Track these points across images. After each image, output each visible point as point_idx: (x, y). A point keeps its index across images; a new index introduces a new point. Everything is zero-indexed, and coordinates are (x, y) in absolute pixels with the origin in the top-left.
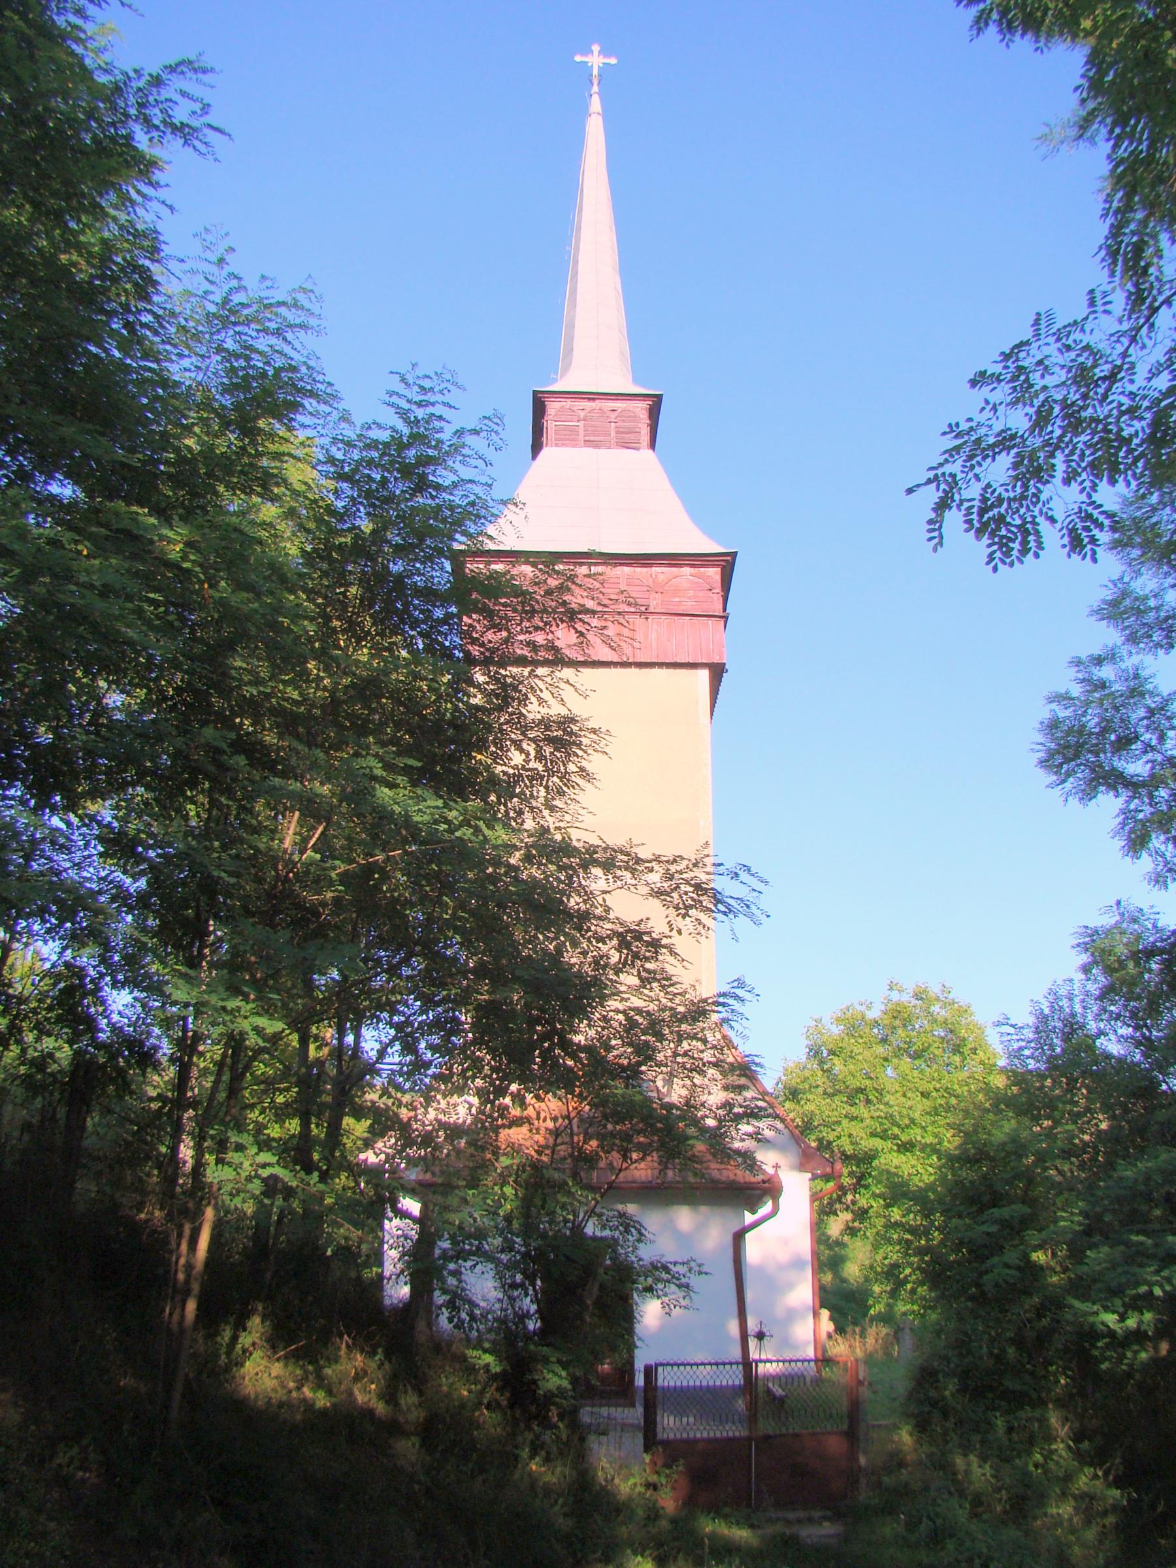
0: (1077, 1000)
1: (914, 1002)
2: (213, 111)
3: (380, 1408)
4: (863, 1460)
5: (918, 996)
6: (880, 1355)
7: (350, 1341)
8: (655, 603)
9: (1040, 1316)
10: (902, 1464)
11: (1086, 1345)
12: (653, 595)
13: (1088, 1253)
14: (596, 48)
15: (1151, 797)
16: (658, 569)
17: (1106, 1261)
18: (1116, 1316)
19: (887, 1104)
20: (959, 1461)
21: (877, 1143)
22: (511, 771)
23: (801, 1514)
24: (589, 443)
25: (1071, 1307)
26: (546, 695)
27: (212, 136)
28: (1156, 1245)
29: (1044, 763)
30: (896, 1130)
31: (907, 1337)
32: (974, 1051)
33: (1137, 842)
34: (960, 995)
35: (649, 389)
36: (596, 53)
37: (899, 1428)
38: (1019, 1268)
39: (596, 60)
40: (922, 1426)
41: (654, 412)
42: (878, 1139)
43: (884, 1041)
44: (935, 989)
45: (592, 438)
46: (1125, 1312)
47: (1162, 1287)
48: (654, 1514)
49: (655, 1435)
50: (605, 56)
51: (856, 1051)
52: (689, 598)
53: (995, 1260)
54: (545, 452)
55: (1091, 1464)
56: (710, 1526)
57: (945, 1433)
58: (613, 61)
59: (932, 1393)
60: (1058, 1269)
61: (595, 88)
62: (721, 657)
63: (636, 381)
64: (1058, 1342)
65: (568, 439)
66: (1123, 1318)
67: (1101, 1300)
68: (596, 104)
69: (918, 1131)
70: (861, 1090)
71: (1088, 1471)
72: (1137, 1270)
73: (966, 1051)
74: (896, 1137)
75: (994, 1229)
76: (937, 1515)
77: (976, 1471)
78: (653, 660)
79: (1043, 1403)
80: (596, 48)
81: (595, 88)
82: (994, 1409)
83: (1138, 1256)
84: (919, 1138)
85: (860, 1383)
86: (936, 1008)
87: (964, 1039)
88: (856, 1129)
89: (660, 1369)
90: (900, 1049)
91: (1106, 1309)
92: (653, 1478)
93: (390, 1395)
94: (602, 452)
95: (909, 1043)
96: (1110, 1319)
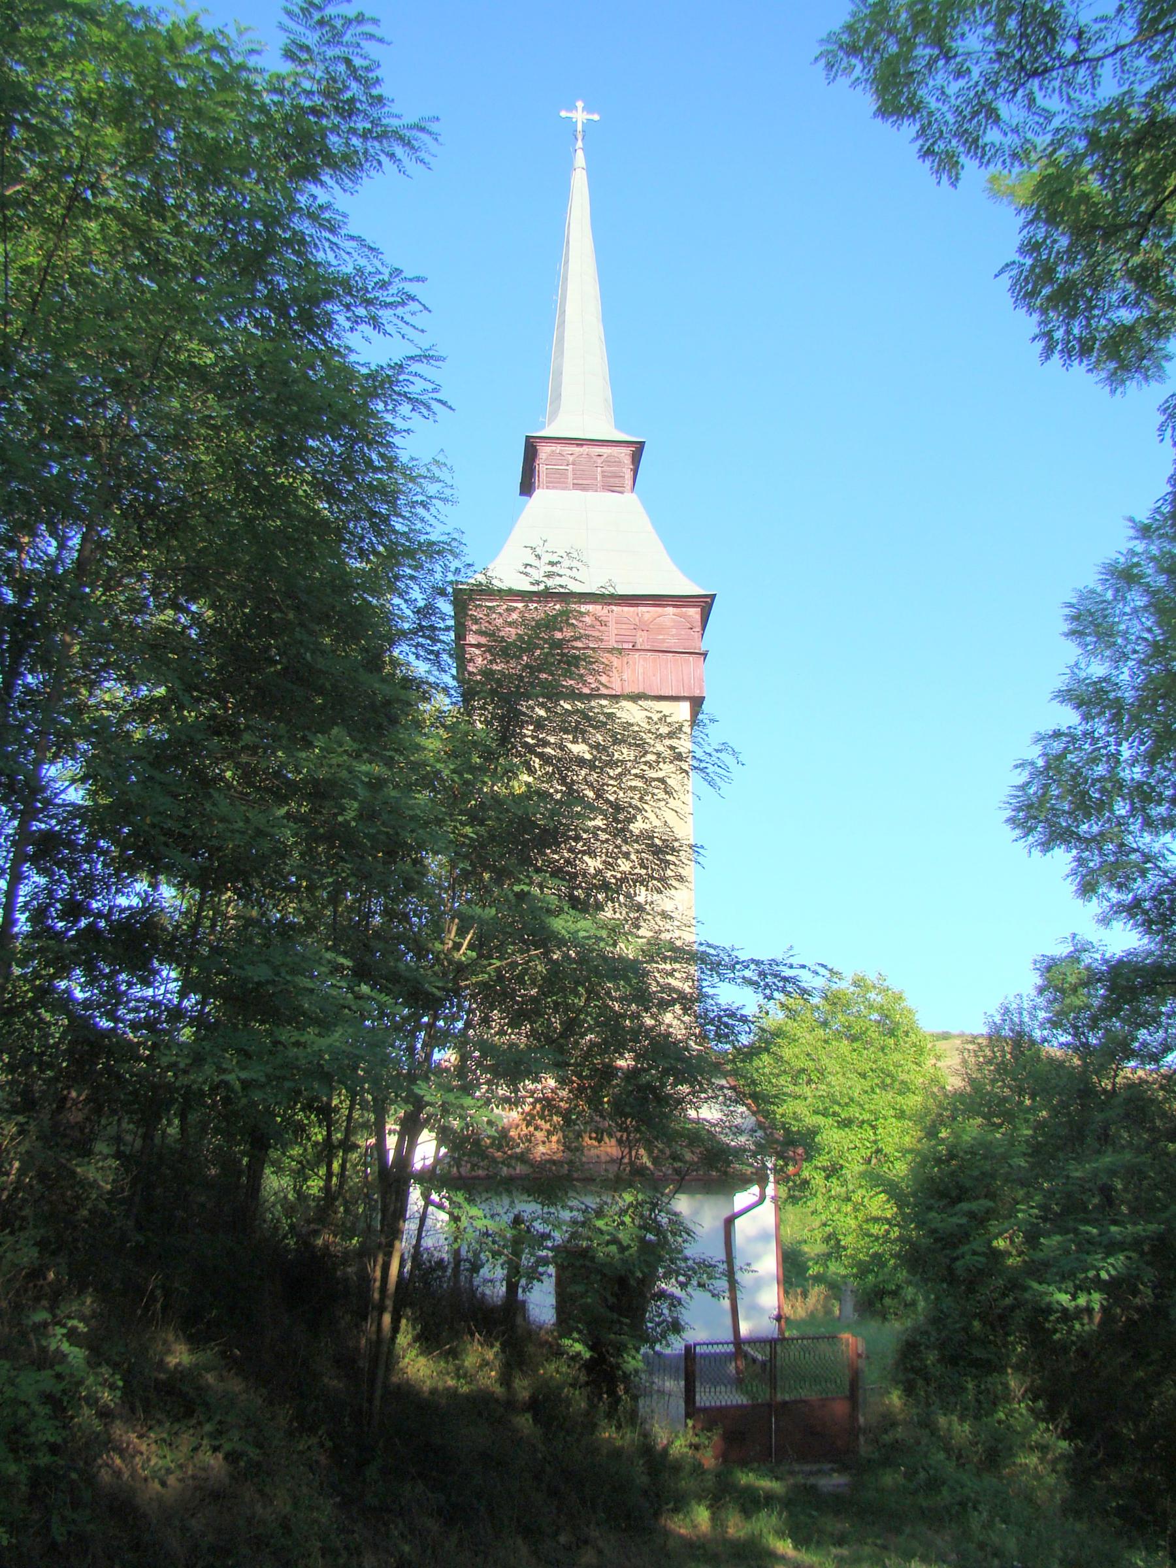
0: (1025, 1013)
1: (852, 989)
2: (443, 391)
3: (498, 1390)
4: (861, 1420)
5: (856, 984)
6: (820, 1314)
7: (482, 1339)
8: (641, 639)
9: (1004, 1295)
10: (894, 1425)
11: (1041, 1319)
12: (640, 633)
13: (1042, 1240)
14: (580, 104)
15: (1100, 849)
17: (1058, 1249)
18: (1069, 1296)
19: (829, 1084)
20: (942, 1421)
21: (820, 1120)
22: (619, 876)
23: (815, 1468)
24: (577, 486)
25: (1030, 1287)
26: (650, 815)
27: (435, 406)
28: (1100, 1235)
29: (1011, 820)
30: (837, 1108)
31: (848, 1299)
32: (907, 1033)
33: (1087, 889)
34: (895, 983)
35: (631, 435)
36: (580, 109)
37: (889, 1393)
38: (984, 1254)
39: (580, 116)
40: (909, 1390)
41: (636, 458)
42: (820, 1117)
43: (825, 1024)
44: (872, 977)
45: (580, 482)
46: (1076, 1293)
47: (1108, 1272)
48: (698, 1469)
49: (694, 1402)
51: (799, 1034)
53: (966, 1248)
54: (538, 493)
55: (1043, 1420)
56: (746, 1478)
57: (927, 1397)
58: (596, 117)
59: (916, 1363)
60: (1014, 1252)
61: (580, 144)
62: (701, 691)
63: (619, 426)
64: (1019, 1316)
65: (558, 482)
66: (1074, 1297)
67: (1055, 1282)
68: (580, 159)
69: (857, 1109)
70: (803, 1070)
71: (1042, 1426)
72: (1086, 1256)
73: (900, 1033)
74: (835, 1114)
75: (964, 1221)
76: (930, 1466)
77: (956, 1426)
79: (1001, 1370)
80: (580, 104)
81: (580, 144)
82: (965, 1375)
83: (1088, 1245)
84: (857, 1115)
85: (859, 1356)
86: (872, 995)
87: (898, 1023)
88: (799, 1107)
90: (840, 1032)
91: (1060, 1290)
92: (696, 1440)
93: (505, 1379)
94: (590, 494)
95: (849, 1027)
96: (1064, 1298)
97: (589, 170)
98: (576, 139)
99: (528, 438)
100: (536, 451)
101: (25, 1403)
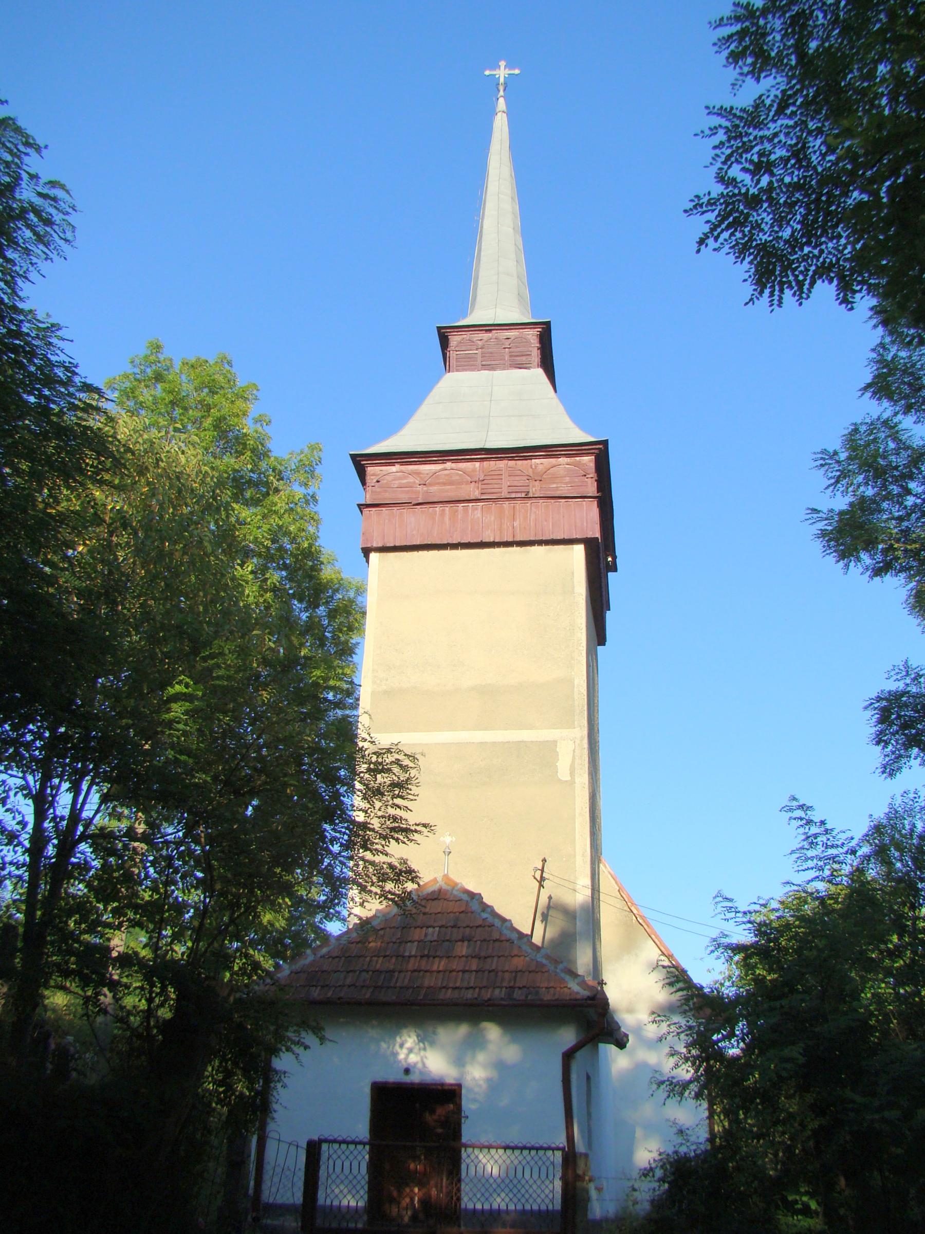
12: (532, 483)
14: (502, 64)
16: (537, 461)
36: (502, 67)
50: (510, 69)
52: (566, 483)
58: (517, 72)
61: (501, 93)
65: (468, 364)
68: (502, 104)
78: (532, 539)
80: (502, 64)
81: (501, 93)
89: (324, 1146)
94: (498, 374)
97: (509, 113)
98: (499, 91)
99: (439, 329)
100: (448, 340)
101: (73, 227)
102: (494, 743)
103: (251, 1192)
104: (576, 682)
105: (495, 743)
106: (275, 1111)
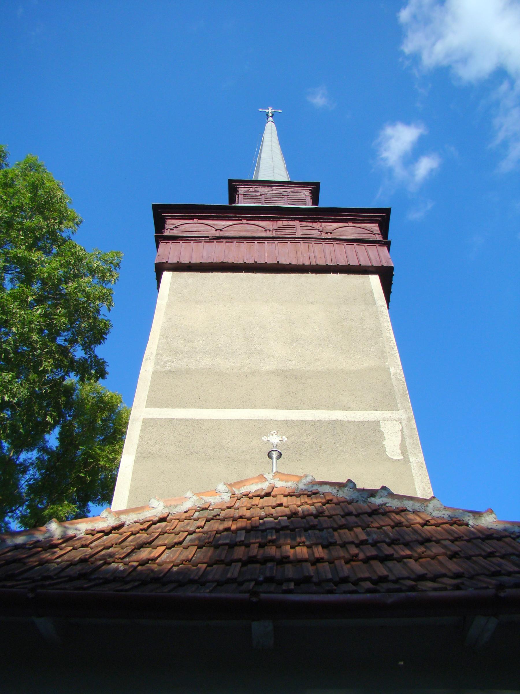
50: (275, 110)
99: (230, 182)
102: (302, 422)
103: (312, 189)
104: (392, 370)
105: (303, 421)
106: (57, 438)
